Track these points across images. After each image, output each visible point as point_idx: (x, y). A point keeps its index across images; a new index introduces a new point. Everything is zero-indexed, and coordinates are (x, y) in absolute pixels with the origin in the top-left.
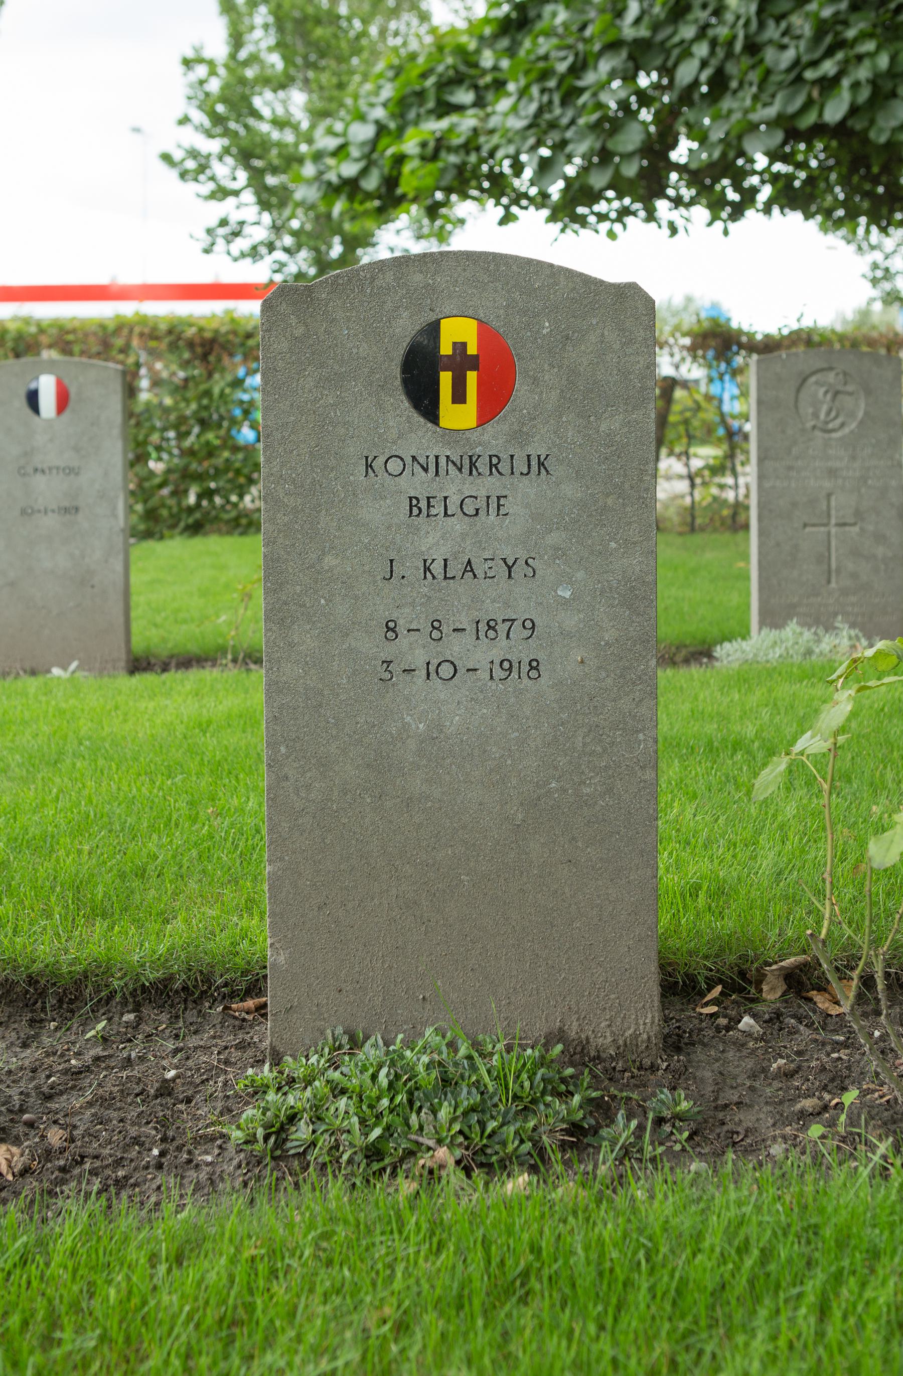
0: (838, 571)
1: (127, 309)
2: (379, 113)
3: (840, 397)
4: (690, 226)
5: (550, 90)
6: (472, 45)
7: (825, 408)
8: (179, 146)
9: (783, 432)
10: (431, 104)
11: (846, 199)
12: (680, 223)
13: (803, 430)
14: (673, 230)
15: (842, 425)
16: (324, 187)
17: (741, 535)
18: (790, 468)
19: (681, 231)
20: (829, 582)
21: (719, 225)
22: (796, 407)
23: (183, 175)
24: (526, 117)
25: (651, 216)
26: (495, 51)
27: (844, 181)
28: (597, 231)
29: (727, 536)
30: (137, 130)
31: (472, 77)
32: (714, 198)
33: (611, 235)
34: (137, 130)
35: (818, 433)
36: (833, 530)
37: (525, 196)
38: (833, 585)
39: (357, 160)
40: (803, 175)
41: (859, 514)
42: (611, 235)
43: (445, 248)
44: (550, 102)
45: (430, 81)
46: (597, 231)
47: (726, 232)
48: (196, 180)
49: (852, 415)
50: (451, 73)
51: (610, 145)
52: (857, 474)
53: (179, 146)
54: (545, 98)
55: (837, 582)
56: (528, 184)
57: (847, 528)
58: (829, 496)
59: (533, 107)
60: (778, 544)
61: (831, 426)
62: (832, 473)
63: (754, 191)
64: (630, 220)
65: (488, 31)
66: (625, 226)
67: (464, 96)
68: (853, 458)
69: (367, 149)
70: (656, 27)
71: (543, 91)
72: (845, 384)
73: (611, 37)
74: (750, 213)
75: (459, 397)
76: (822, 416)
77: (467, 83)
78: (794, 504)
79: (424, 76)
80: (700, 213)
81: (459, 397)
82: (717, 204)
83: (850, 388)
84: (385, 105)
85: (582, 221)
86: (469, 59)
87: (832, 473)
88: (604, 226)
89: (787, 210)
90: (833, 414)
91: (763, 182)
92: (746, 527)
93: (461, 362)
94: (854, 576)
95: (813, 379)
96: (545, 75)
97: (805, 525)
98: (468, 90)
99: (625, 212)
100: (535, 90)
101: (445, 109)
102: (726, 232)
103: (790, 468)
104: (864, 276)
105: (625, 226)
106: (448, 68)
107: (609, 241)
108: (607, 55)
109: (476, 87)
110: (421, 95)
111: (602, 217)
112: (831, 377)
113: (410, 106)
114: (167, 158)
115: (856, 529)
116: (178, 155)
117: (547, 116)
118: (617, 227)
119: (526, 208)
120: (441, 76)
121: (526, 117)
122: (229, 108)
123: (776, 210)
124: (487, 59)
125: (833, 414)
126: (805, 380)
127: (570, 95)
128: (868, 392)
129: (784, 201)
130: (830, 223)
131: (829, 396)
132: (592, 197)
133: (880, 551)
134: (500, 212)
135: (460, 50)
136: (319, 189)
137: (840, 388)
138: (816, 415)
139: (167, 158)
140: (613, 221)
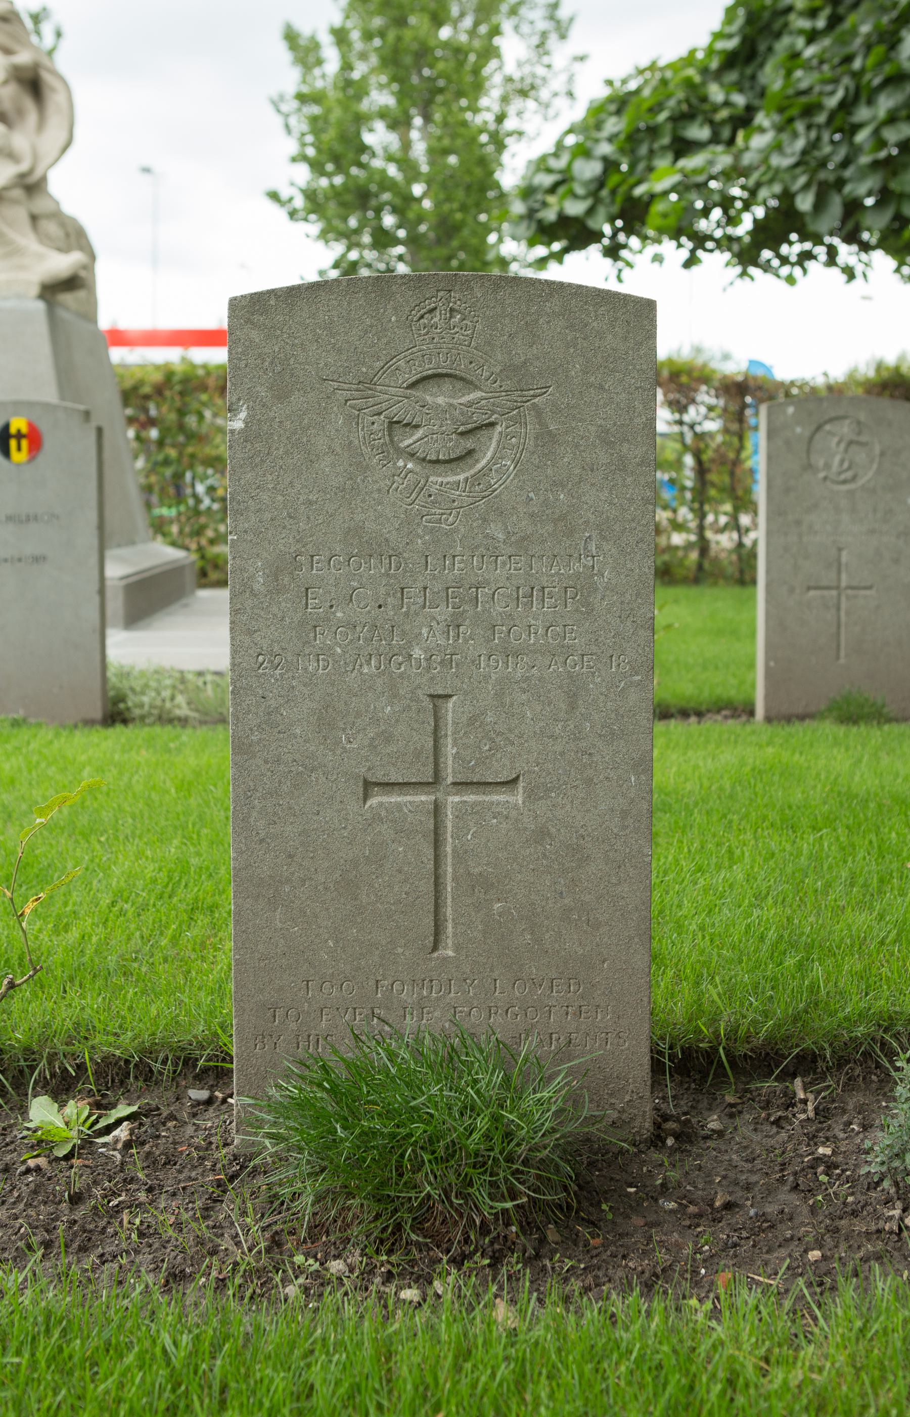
1: (171, 355)
2: (605, 149)
5: (819, 127)
6: (697, 79)
7: (837, 459)
8: (292, 184)
10: (666, 140)
12: (859, 269)
16: (534, 226)
17: (747, 591)
23: (293, 214)
24: (793, 154)
25: (832, 260)
26: (722, 85)
29: (737, 590)
30: (146, 170)
31: (705, 112)
34: (146, 170)
37: (710, 238)
39: (584, 198)
44: (818, 139)
45: (662, 117)
48: (306, 220)
50: (685, 107)
51: (894, 185)
53: (292, 184)
54: (813, 134)
56: (715, 225)
59: (800, 144)
64: (810, 265)
65: (714, 64)
66: (805, 271)
67: (699, 132)
69: (593, 187)
71: (809, 127)
72: (859, 433)
73: (888, 69)
75: (19, 449)
77: (700, 119)
81: (19, 449)
84: (610, 140)
88: (785, 271)
92: (754, 582)
93: (19, 436)
95: (828, 427)
96: (809, 111)
98: (701, 125)
99: (807, 256)
100: (800, 126)
101: (683, 147)
105: (805, 271)
106: (679, 102)
108: (889, 89)
109: (711, 123)
110: (653, 131)
111: (784, 260)
113: (641, 142)
114: (274, 196)
116: (285, 192)
117: (816, 154)
118: (797, 271)
119: (711, 251)
120: (673, 110)
121: (793, 154)
122: (335, 144)
131: (843, 446)
134: (684, 254)
135: (689, 84)
136: (528, 228)
138: (827, 466)
139: (274, 196)
140: (793, 265)
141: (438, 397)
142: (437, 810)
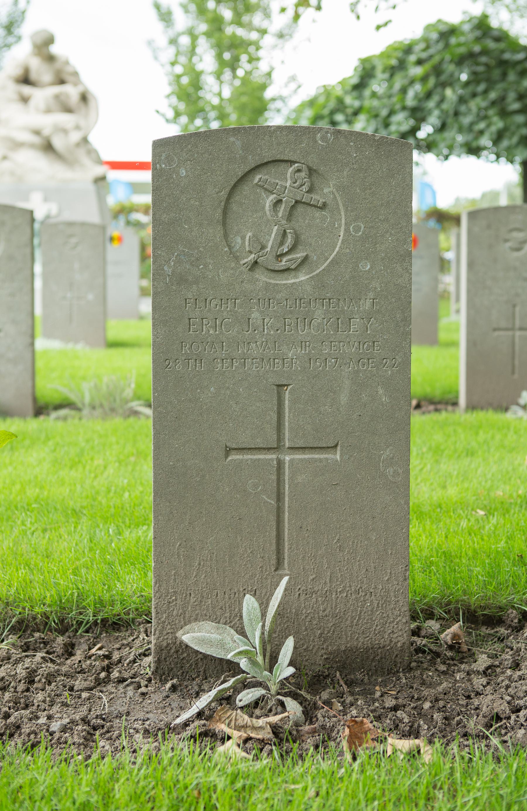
61: (284, 263)
70: (420, 100)
79: (324, 107)
86: (340, 101)
90: (289, 241)
97: (228, 451)
124: (348, 100)
125: (289, 241)
127: (387, 125)
131: (282, 210)
141: (515, 234)
142: (280, 464)
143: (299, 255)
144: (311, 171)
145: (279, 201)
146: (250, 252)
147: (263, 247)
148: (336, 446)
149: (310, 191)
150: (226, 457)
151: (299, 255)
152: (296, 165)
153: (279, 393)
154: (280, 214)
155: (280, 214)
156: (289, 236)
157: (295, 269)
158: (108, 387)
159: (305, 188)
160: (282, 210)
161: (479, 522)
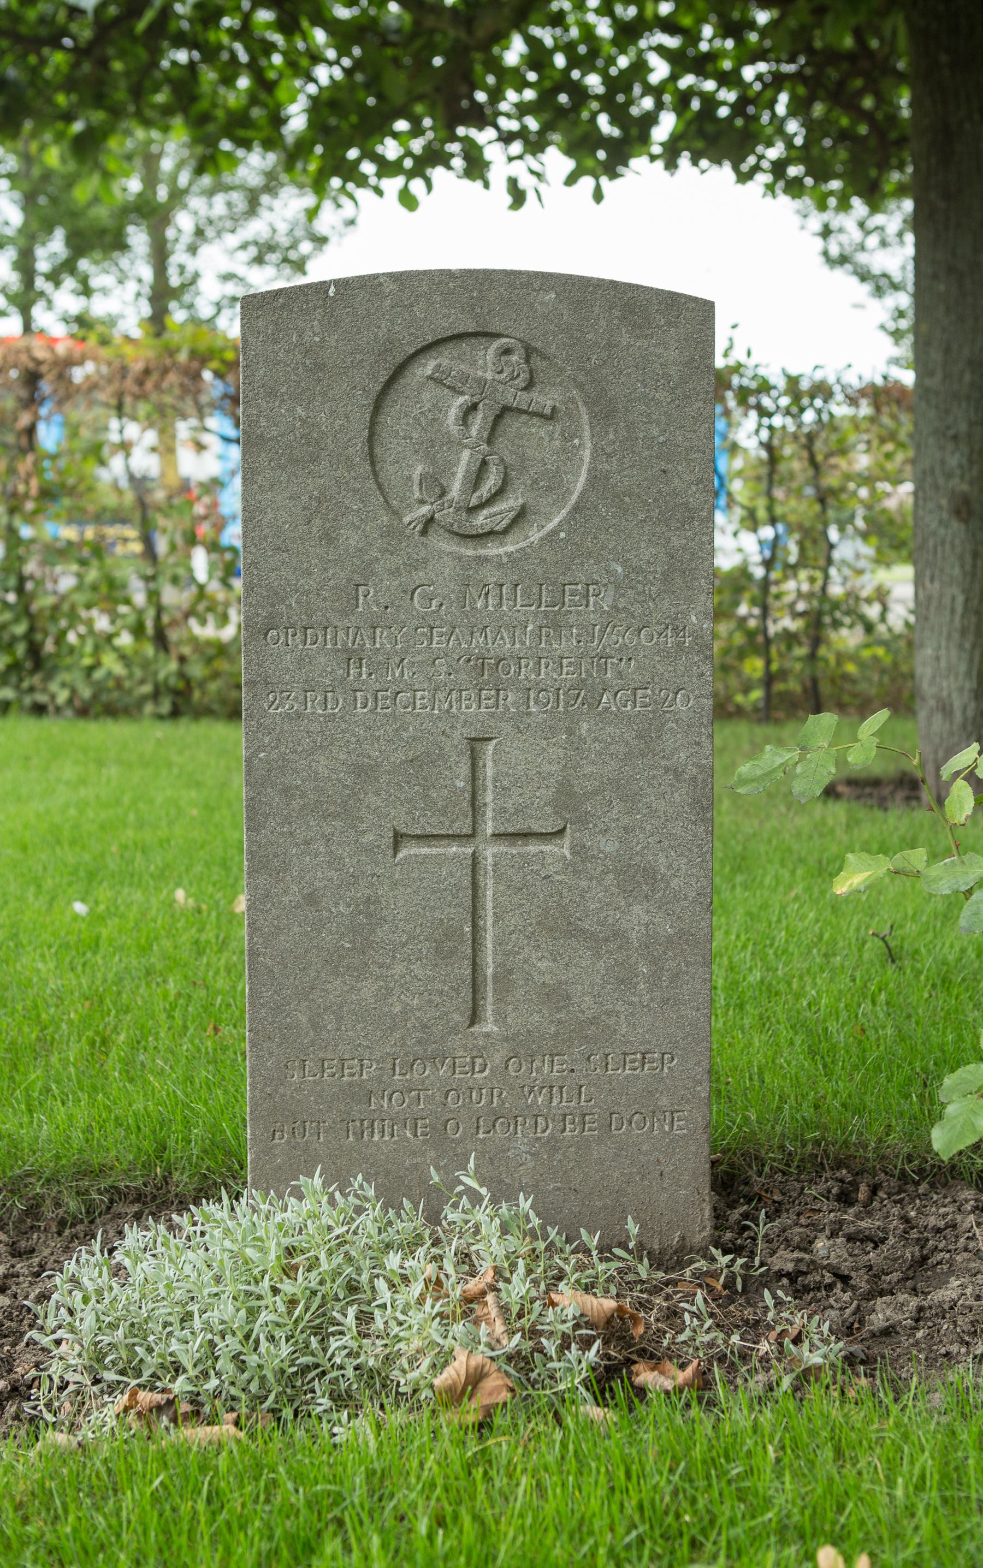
0: (504, 980)
3: (513, 425)
4: (542, 188)
9: (328, 538)
11: (806, 146)
12: (527, 182)
13: (392, 533)
14: (518, 197)
15: (521, 516)
18: (351, 656)
19: (531, 197)
20: (474, 1017)
21: (587, 182)
22: (372, 459)
25: (476, 167)
27: (799, 108)
28: (379, 192)
32: (579, 132)
33: (408, 201)
35: (442, 543)
36: (490, 853)
38: (489, 1026)
40: (729, 96)
41: (567, 800)
42: (408, 201)
43: (301, 281)
46: (379, 192)
47: (598, 196)
49: (553, 484)
52: (568, 676)
55: (500, 1018)
57: (533, 848)
58: (476, 743)
60: (312, 899)
61: (481, 520)
62: (486, 671)
63: (650, 119)
64: (438, 173)
66: (429, 186)
68: (555, 625)
74: (639, 163)
76: (455, 490)
78: (364, 772)
80: (556, 161)
82: (582, 145)
83: (544, 399)
85: (351, 173)
87: (486, 671)
88: (392, 185)
89: (704, 163)
90: (491, 482)
91: (659, 105)
94: (555, 996)
95: (428, 366)
97: (398, 839)
102: (598, 196)
103: (351, 656)
104: (882, 327)
105: (429, 186)
107: (403, 211)
111: (387, 168)
112: (484, 362)
115: (563, 848)
118: (417, 186)
123: (684, 160)
125: (491, 482)
126: (400, 370)
128: (605, 412)
129: (699, 144)
130: (781, 184)
131: (478, 422)
132: (373, 126)
133: (637, 917)
137: (513, 396)
138: (436, 486)
143: (510, 503)
144: (529, 352)
145: (474, 407)
146: (422, 502)
147: (443, 493)
148: (561, 832)
149: (529, 386)
150: (395, 856)
151: (510, 503)
152: (504, 340)
153: (473, 750)
154: (474, 432)
155: (474, 432)
156: (493, 469)
157: (505, 531)
158: (911, 612)
159: (520, 382)
160: (478, 422)
161: (124, 377)
